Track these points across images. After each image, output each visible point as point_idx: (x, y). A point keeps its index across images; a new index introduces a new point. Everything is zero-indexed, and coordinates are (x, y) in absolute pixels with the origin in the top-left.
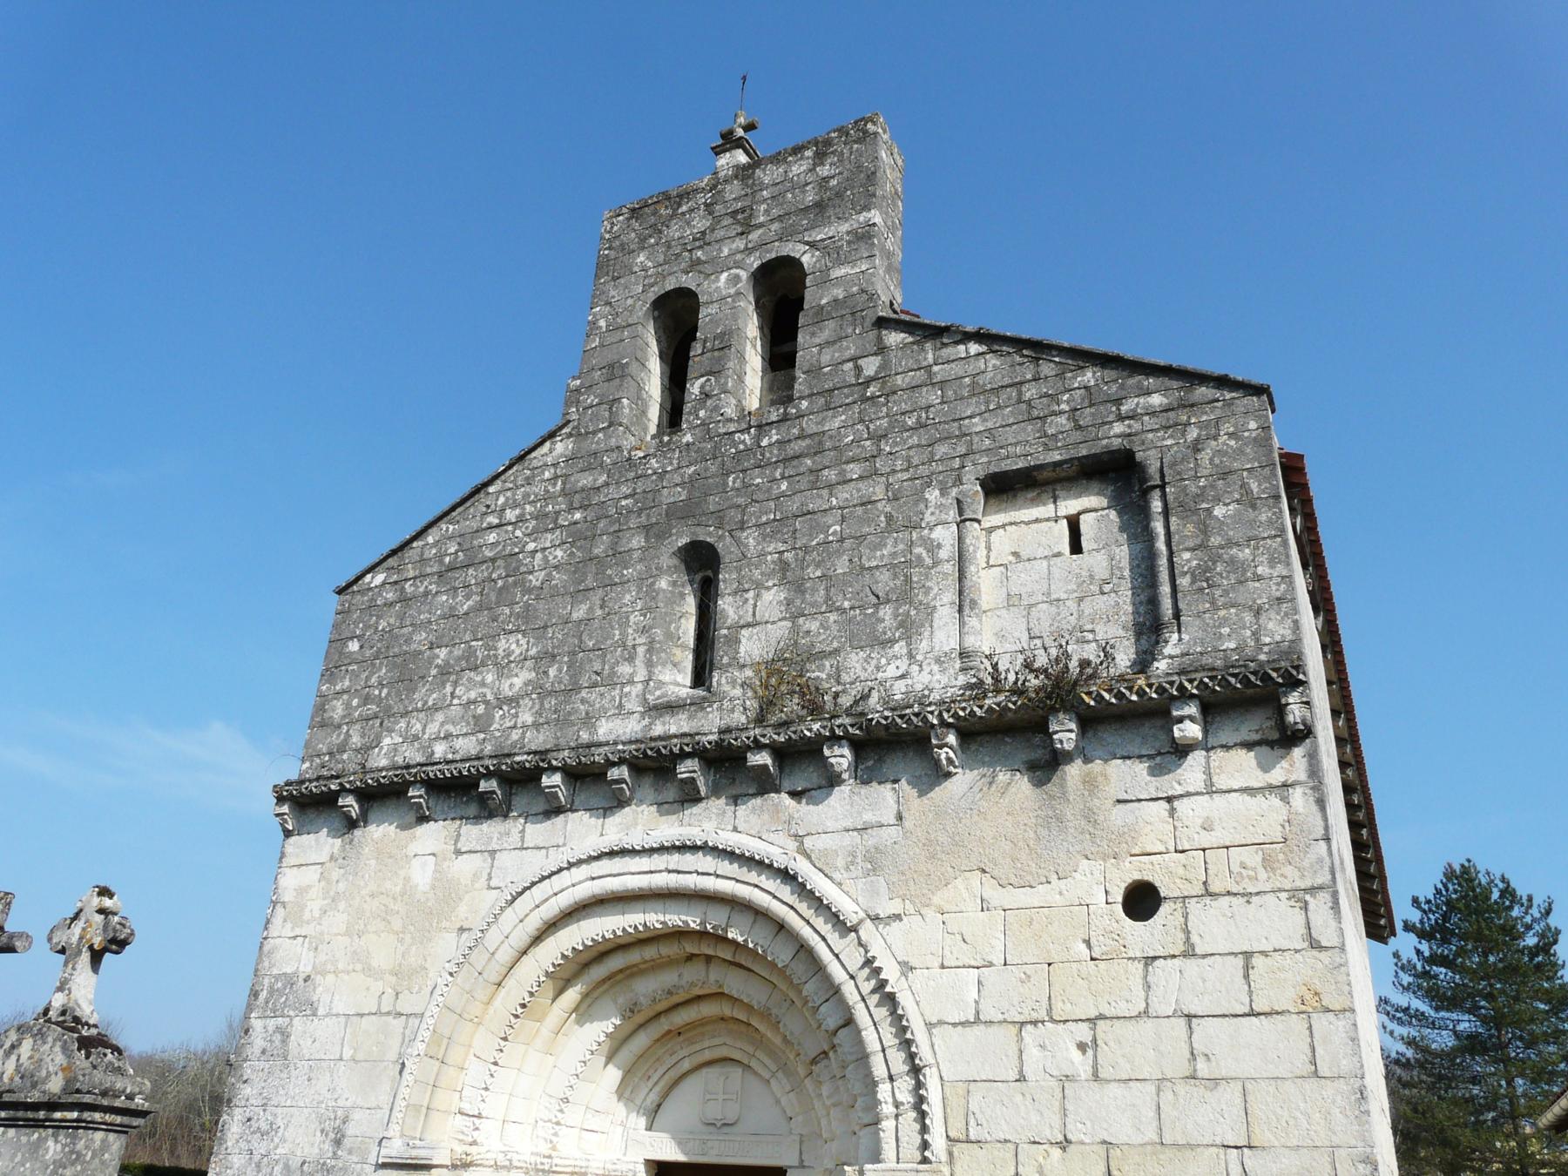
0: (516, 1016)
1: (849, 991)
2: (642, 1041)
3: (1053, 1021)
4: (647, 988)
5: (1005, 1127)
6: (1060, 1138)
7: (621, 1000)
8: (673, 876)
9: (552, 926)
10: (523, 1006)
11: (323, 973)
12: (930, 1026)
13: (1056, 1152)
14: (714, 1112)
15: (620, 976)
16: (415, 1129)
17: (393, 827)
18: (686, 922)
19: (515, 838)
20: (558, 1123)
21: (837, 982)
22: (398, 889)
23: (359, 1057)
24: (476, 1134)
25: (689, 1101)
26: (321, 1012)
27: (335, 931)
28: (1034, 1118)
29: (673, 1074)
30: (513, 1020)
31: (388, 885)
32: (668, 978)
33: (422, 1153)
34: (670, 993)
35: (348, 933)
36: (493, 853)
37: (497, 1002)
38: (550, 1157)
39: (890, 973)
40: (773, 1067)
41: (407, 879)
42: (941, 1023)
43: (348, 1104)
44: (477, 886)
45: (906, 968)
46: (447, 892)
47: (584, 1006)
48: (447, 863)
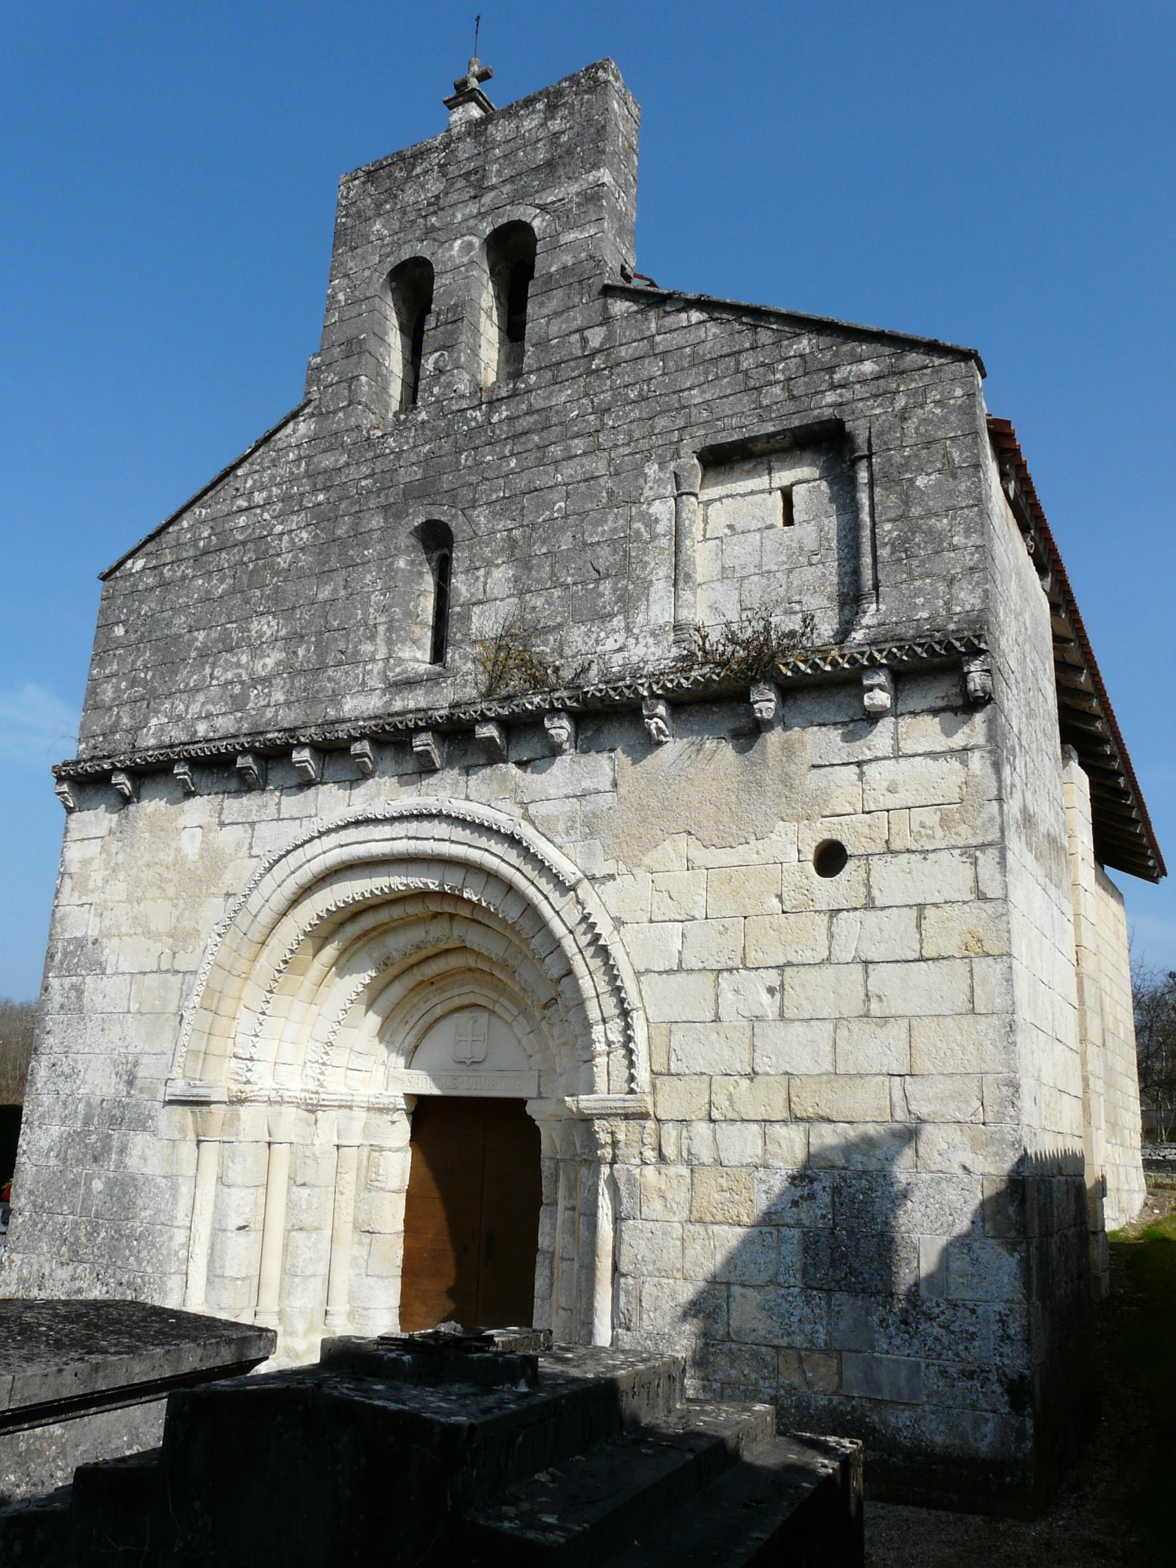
0: (280, 971)
1: (569, 945)
2: (397, 990)
3: (746, 968)
4: (398, 943)
5: (701, 1062)
6: (749, 1070)
7: (375, 955)
11: (109, 936)
12: (638, 974)
13: (745, 1083)
15: (374, 934)
16: (195, 1071)
19: (272, 810)
20: (324, 1064)
23: (144, 1010)
24: (249, 1074)
27: (117, 898)
28: (727, 1053)
29: (428, 1019)
31: (162, 855)
33: (202, 1091)
34: (419, 947)
36: (252, 824)
38: (317, 1093)
39: (604, 928)
42: (648, 971)
43: (138, 1050)
44: (240, 855)
46: (214, 861)
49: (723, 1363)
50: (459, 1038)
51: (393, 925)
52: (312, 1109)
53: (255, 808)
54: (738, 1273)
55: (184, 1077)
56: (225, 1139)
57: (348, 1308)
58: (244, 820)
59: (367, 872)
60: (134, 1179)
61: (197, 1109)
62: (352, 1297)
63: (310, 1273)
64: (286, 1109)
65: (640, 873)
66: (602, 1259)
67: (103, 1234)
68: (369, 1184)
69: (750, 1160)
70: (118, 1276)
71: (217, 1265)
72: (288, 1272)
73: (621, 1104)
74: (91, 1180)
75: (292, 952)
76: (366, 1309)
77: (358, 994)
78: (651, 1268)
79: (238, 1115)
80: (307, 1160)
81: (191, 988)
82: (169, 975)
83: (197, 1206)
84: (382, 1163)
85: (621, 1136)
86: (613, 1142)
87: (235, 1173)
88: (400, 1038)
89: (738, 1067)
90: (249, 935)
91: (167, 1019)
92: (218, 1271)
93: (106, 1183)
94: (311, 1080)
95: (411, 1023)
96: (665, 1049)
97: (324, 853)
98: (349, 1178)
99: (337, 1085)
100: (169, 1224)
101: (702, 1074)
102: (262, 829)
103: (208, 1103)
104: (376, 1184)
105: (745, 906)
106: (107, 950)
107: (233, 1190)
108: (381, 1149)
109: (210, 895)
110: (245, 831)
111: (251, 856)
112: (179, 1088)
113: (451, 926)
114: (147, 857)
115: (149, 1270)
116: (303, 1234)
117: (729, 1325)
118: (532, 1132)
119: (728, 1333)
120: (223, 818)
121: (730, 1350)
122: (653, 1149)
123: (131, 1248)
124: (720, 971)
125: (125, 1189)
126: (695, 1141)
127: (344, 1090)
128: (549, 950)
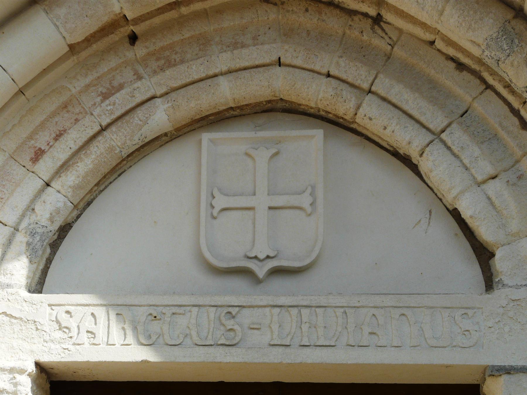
14: (232, 242)
25: (161, 212)
29: (120, 140)
40: (436, 120)
50: (221, 202)
52: (48, 185)
95: (61, 152)
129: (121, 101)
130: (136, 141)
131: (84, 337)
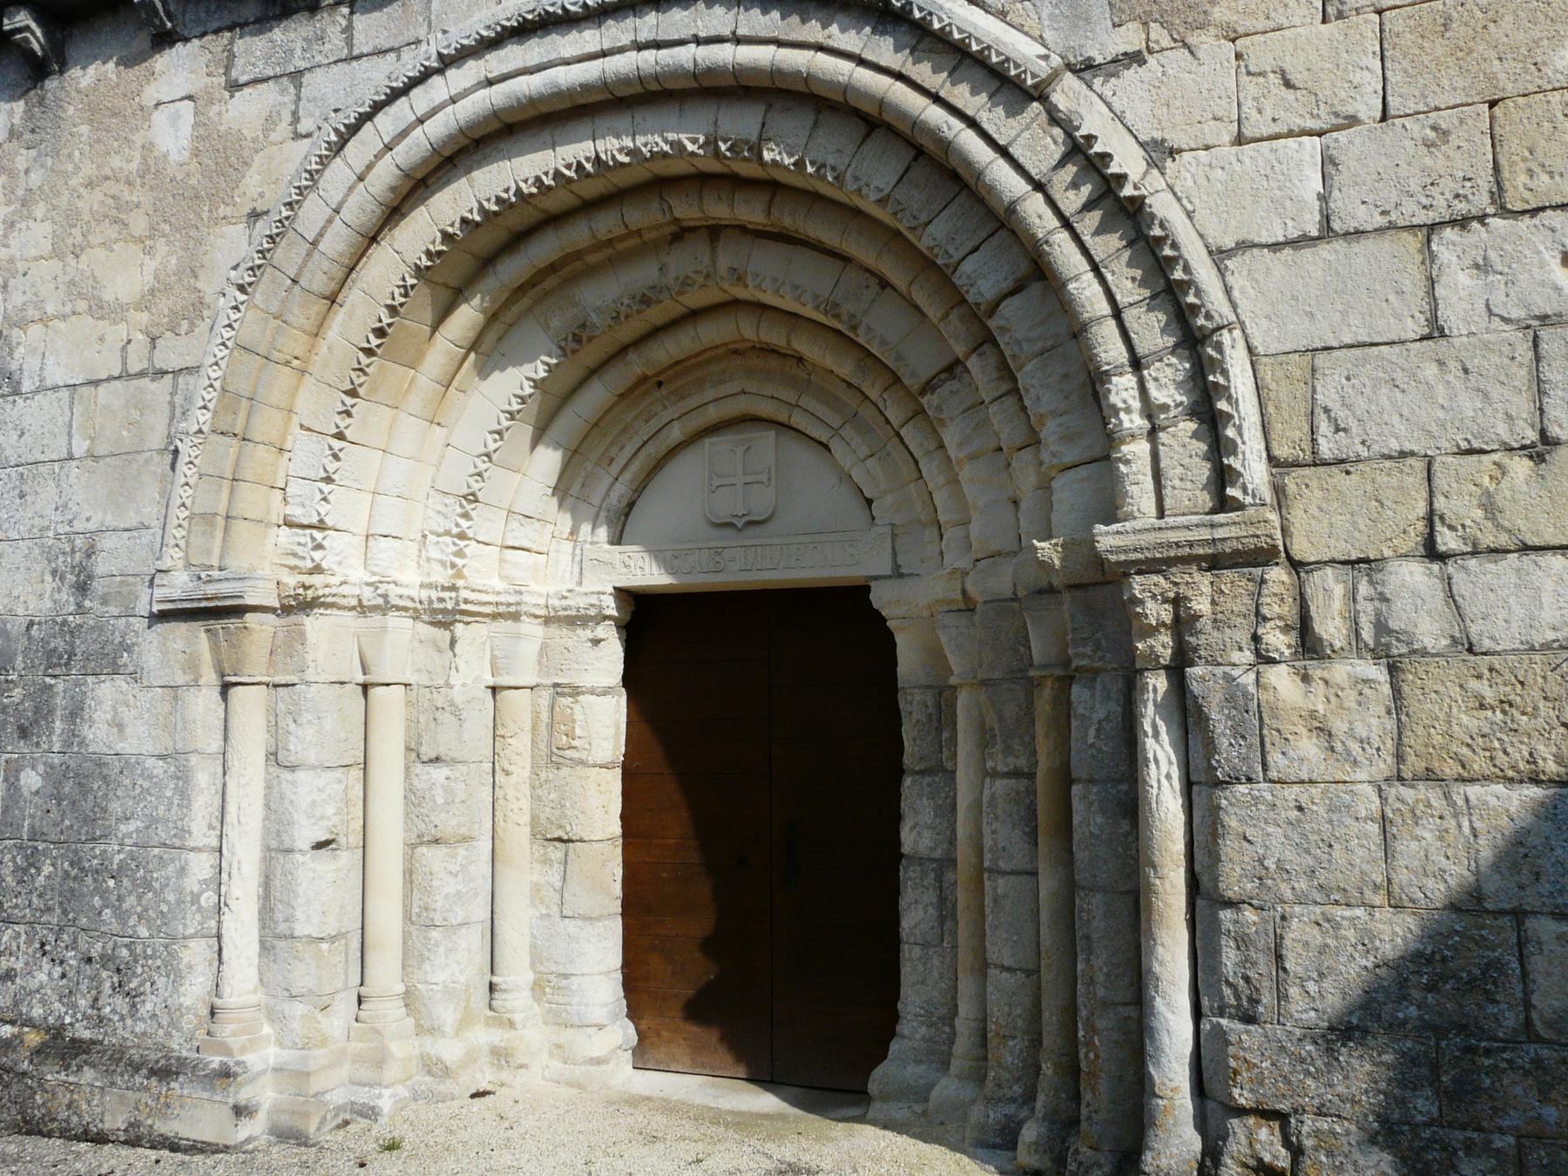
0: (369, 352)
1: (1036, 213)
2: (597, 396)
3: (1505, 212)
4: (600, 296)
5: (1400, 427)
6: (1532, 436)
7: (555, 323)
8: (649, 56)
9: (419, 184)
10: (380, 332)
11: (23, 324)
12: (1219, 256)
13: (1521, 467)
14: (729, 505)
15: (551, 282)
16: (209, 552)
17: (111, 65)
18: (678, 146)
19: (335, 43)
20: (462, 536)
21: (1007, 197)
22: (134, 166)
23: (101, 449)
24: (317, 555)
25: (683, 493)
26: (26, 386)
27: (33, 252)
28: (1468, 404)
29: (655, 450)
30: (365, 360)
31: (116, 162)
32: (642, 274)
33: (225, 588)
34: (646, 301)
35: (56, 254)
36: (296, 76)
37: (333, 332)
38: (453, 588)
39: (1127, 161)
40: (835, 421)
41: (148, 147)
42: (1244, 246)
43: (92, 526)
44: (274, 137)
45: (1159, 152)
46: (221, 156)
47: (491, 337)
48: (215, 108)
49: (1519, 1090)
50: (716, 482)
51: (592, 259)
52: (445, 618)
53: (299, 44)
54: (1545, 887)
55: (188, 565)
56: (279, 679)
57: (530, 976)
58: (278, 70)
59: (546, 135)
60: (100, 764)
61: (218, 625)
62: (536, 959)
63: (459, 920)
64: (394, 621)
65: (1205, 41)
66: (1162, 871)
67: (47, 869)
68: (556, 753)
69: (1550, 636)
70: (83, 946)
71: (279, 916)
72: (418, 921)
73: (1206, 534)
74: (18, 771)
75: (393, 310)
76: (566, 976)
77: (523, 400)
78: (1302, 885)
79: (302, 634)
80: (438, 714)
81: (188, 399)
82: (145, 382)
83: (231, 808)
84: (578, 716)
85: (1201, 605)
86: (1177, 619)
87: (303, 742)
88: (602, 488)
89: (1502, 430)
90: (303, 282)
91: (147, 462)
92: (282, 928)
93: (46, 776)
94: (437, 567)
96: (1303, 408)
97: (453, 100)
98: (520, 748)
99: (486, 576)
100: (178, 844)
101: (1403, 455)
102: (316, 83)
103: (239, 611)
104: (568, 753)
105: (1491, 77)
106: (22, 349)
107: (301, 775)
108: (575, 691)
109: (217, 221)
110: (283, 92)
111: (298, 136)
112: (179, 586)
113: (713, 249)
114: (88, 169)
115: (143, 932)
116: (441, 851)
117: (1528, 1005)
118: (877, 639)
119: (1528, 1023)
120: (234, 74)
121: (1537, 1062)
122: (1286, 629)
123: (104, 893)
124: (1432, 228)
125: (84, 786)
126: (1398, 604)
127: (500, 585)
128: (970, 245)
129: (655, 424)
130: (664, 449)
131: (639, 572)
